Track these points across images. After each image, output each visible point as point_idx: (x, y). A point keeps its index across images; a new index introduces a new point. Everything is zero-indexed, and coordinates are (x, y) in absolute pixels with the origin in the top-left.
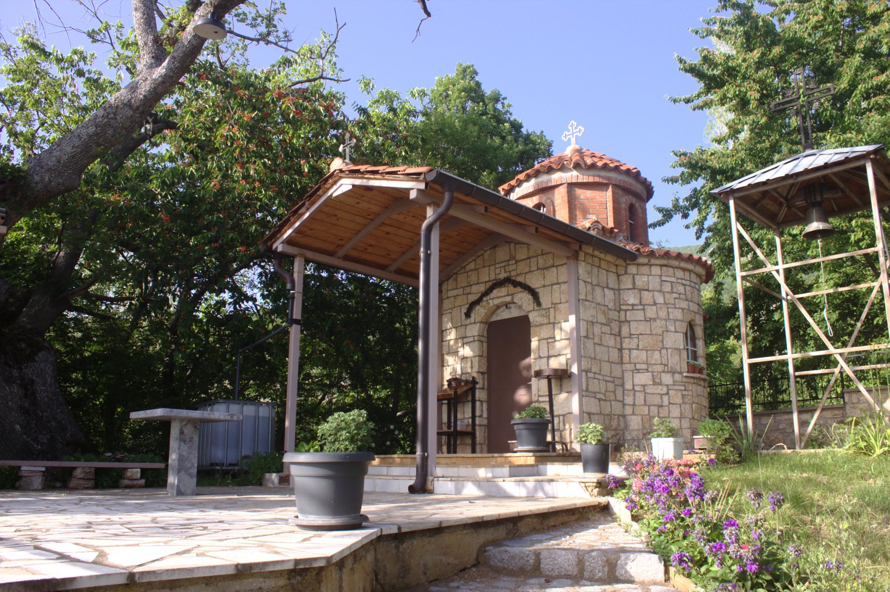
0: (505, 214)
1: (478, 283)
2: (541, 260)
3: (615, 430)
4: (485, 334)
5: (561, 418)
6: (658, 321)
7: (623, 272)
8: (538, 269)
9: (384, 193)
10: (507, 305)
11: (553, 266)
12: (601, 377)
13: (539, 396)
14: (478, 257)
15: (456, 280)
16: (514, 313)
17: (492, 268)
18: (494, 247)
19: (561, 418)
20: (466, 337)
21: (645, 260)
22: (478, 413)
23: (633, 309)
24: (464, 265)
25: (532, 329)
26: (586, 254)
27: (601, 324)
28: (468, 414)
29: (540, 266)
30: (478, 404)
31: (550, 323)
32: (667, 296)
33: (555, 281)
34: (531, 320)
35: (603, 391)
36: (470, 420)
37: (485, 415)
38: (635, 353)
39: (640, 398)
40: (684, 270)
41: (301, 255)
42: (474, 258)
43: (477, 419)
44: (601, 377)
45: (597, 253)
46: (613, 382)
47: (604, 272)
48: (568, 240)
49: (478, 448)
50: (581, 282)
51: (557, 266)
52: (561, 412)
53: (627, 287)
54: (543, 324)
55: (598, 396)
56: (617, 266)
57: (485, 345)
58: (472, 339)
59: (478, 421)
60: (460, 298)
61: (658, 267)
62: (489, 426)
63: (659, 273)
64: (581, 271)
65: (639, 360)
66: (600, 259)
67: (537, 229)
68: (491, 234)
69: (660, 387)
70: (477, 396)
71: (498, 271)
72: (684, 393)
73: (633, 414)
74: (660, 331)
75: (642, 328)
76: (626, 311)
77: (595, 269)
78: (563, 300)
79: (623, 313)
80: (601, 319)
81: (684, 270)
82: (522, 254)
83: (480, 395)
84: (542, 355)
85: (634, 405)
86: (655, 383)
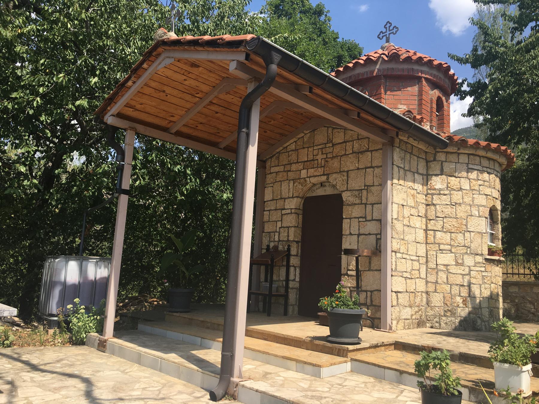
0: (329, 97)
1: (298, 162)
2: (356, 146)
3: (418, 306)
4: (301, 207)
5: (369, 293)
6: (463, 206)
7: (432, 159)
8: (353, 152)
9: (528, 320)
10: (322, 184)
12: (408, 257)
13: (348, 270)
14: (299, 139)
15: (278, 158)
16: (328, 191)
17: (310, 149)
18: (314, 130)
19: (369, 293)
20: (284, 209)
21: (454, 149)
22: (291, 277)
23: (440, 194)
24: (285, 145)
25: (344, 207)
26: (401, 140)
27: (411, 207)
28: (283, 276)
29: (355, 149)
30: (292, 269)
31: (362, 204)
32: (474, 182)
33: (369, 165)
34: (344, 200)
35: (409, 270)
36: (284, 283)
37: (297, 279)
38: (439, 234)
39: (443, 276)
40: (489, 159)
41: (132, 128)
42: (295, 139)
43: (291, 283)
44: (408, 257)
45: (411, 141)
46: (418, 261)
47: (415, 158)
48: (387, 126)
49: (290, 309)
50: (395, 167)
51: (372, 151)
52: (369, 288)
53: (435, 173)
54: (355, 204)
55: (405, 275)
56: (426, 152)
57: (301, 216)
58: (289, 211)
59: (291, 284)
61: (466, 155)
62: (301, 290)
63: (467, 161)
64: (396, 157)
65: (443, 241)
66: (412, 146)
67: (359, 113)
68: (311, 117)
69: (463, 268)
70: (291, 262)
71: (315, 152)
72: (484, 274)
73: (435, 291)
74: (463, 215)
75: (448, 210)
76: (433, 194)
77: (408, 156)
78: (376, 183)
79: (369, 207)
80: (411, 202)
81: (489, 159)
82: (339, 138)
83: (295, 261)
84: (352, 232)
85: (437, 282)
86: (457, 264)
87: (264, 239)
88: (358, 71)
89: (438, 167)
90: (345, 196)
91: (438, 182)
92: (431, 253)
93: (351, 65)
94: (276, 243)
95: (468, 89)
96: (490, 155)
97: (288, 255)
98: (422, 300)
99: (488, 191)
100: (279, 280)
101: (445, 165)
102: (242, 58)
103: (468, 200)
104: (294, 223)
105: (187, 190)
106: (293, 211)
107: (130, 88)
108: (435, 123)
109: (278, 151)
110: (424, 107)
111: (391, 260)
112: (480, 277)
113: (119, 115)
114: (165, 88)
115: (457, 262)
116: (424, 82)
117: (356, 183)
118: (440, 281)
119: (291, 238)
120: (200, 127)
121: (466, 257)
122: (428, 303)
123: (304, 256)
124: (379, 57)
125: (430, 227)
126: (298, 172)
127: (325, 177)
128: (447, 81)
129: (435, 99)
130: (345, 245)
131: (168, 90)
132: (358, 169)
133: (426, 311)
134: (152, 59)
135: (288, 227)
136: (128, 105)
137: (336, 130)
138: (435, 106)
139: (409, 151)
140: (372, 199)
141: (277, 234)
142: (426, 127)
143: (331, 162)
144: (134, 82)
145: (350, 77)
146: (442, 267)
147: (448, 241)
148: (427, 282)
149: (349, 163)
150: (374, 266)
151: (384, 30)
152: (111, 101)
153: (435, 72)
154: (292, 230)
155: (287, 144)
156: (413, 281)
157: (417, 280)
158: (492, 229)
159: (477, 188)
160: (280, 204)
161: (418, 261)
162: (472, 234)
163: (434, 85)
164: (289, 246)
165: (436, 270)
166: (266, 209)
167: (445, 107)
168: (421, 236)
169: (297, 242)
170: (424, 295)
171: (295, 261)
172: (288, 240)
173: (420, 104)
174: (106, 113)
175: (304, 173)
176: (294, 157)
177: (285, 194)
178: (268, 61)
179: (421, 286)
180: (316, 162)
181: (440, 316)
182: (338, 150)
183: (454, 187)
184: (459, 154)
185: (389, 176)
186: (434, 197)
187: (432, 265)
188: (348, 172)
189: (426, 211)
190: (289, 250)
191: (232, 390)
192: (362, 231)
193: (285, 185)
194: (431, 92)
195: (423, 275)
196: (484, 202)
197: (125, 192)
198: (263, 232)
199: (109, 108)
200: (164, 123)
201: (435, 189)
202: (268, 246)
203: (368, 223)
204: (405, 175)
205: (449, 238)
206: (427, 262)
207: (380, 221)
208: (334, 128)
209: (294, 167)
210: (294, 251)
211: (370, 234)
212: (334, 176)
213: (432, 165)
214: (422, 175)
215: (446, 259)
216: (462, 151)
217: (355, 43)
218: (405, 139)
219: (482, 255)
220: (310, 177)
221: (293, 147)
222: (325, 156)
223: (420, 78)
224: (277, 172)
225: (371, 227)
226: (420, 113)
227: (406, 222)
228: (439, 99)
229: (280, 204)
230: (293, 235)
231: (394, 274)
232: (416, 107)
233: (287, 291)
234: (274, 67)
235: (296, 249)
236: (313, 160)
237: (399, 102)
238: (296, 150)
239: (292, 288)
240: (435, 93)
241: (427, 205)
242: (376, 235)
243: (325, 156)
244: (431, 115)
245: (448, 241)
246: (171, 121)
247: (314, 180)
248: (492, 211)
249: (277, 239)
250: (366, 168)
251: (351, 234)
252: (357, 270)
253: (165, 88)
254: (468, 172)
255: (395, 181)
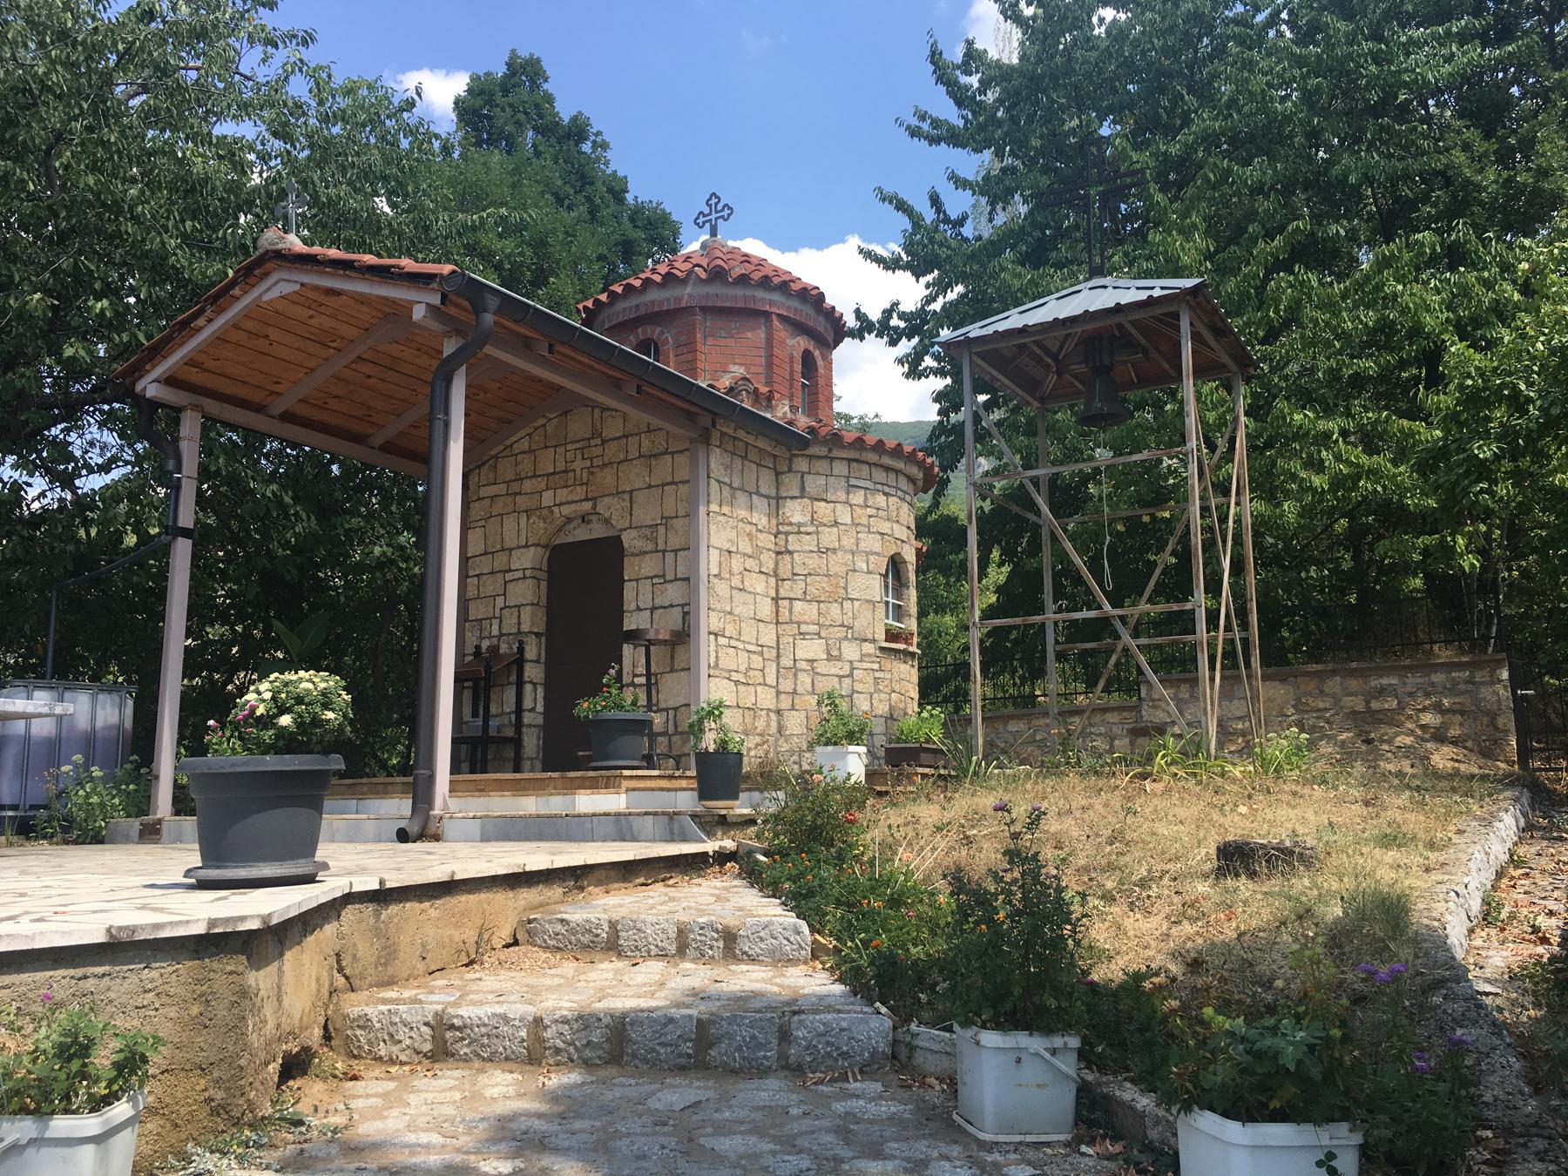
1: (535, 476)
4: (545, 567)
8: (641, 456)
10: (584, 519)
11: (666, 453)
12: (741, 646)
13: (635, 676)
16: (597, 531)
18: (566, 413)
20: (510, 571)
21: (823, 451)
22: (527, 704)
23: (799, 533)
24: (508, 442)
26: (723, 434)
28: (510, 704)
29: (644, 450)
30: (528, 688)
33: (669, 479)
34: (626, 545)
35: (743, 668)
37: (540, 708)
38: (798, 606)
39: (805, 680)
42: (528, 430)
43: (526, 714)
45: (741, 434)
46: (762, 653)
48: (694, 409)
51: (673, 453)
52: (671, 704)
53: (791, 494)
55: (735, 676)
57: (544, 585)
58: (520, 574)
59: (527, 718)
60: (500, 502)
64: (713, 465)
69: (839, 664)
71: (570, 456)
72: (877, 675)
73: (793, 708)
74: (841, 570)
75: (814, 562)
76: (787, 534)
77: (738, 462)
79: (670, 557)
81: (887, 469)
83: (533, 672)
85: (795, 692)
86: (830, 657)
87: (468, 634)
88: (653, 295)
89: (796, 482)
90: (628, 539)
91: (796, 512)
92: (783, 640)
93: (637, 283)
94: (495, 641)
95: (902, 324)
96: (886, 461)
97: (519, 661)
98: (768, 725)
99: (885, 527)
100: (503, 713)
101: (809, 479)
102: (436, 300)
103: (848, 542)
104: (530, 598)
105: (296, 535)
106: (528, 573)
107: (199, 330)
108: (798, 401)
109: (493, 453)
110: (776, 369)
111: (707, 649)
112: (870, 680)
113: (170, 381)
114: (270, 331)
115: (829, 654)
116: (776, 322)
117: (646, 513)
118: (800, 689)
119: (525, 628)
120: (332, 404)
121: (845, 644)
122: (780, 730)
123: (552, 663)
124: (690, 272)
125: (783, 593)
126: (537, 496)
127: (590, 504)
128: (822, 320)
129: (798, 355)
130: (629, 624)
131: (275, 335)
132: (650, 486)
133: (776, 745)
134: (251, 280)
135: (519, 607)
136: (191, 362)
137: (607, 414)
138: (798, 367)
139: (743, 454)
140: (674, 542)
141: (495, 622)
142: (781, 412)
143: (600, 475)
144: (210, 321)
145: (637, 306)
146: (803, 665)
147: (815, 617)
148: (778, 693)
149: (634, 476)
150: (678, 664)
151: (707, 211)
152: (156, 352)
153: (796, 304)
154: (526, 612)
155: (513, 439)
156: (752, 689)
157: (759, 688)
158: (898, 596)
159: (864, 521)
160: (500, 561)
161: (762, 653)
162: (856, 604)
163: (799, 328)
164: (521, 642)
165: (795, 671)
166: (471, 573)
167: (821, 371)
168: (766, 609)
169: (538, 635)
170: (773, 716)
171: (533, 672)
172: (519, 632)
173: (770, 365)
174: (141, 377)
175: (548, 498)
176: (526, 466)
177: (510, 539)
178: (478, 309)
179: (767, 699)
180: (571, 475)
181: (801, 751)
182: (612, 451)
183: (825, 520)
184: (832, 459)
185: (702, 498)
186: (790, 538)
187: (786, 661)
188: (631, 492)
189: (777, 564)
190: (521, 650)
191: (432, 829)
192: (658, 602)
193: (509, 522)
194: (791, 342)
195: (771, 680)
196: (877, 547)
197: (186, 533)
198: (467, 620)
199: (148, 367)
200: (256, 397)
201: (791, 524)
202: (478, 647)
203: (669, 586)
204: (733, 496)
205: (815, 611)
206: (778, 656)
207: (688, 579)
208: (604, 410)
209: (528, 485)
210: (531, 653)
211: (672, 606)
212: (607, 500)
213: (786, 479)
214: (768, 497)
215: (811, 649)
216: (835, 453)
217: (663, 210)
218: (730, 431)
219: (874, 641)
220: (561, 504)
221: (524, 444)
222: (588, 463)
223: (767, 315)
224: (492, 498)
225: (673, 593)
226: (769, 382)
227: (736, 582)
228: (807, 357)
229: (500, 561)
230: (532, 620)
231: (712, 672)
232: (761, 370)
233: (519, 732)
234: (489, 318)
235: (535, 649)
236: (565, 471)
237: (724, 366)
238: (531, 451)
239: (530, 726)
240: (801, 343)
241: (778, 553)
242: (683, 606)
243: (588, 463)
244: (792, 386)
245: (815, 617)
246: (272, 393)
247: (566, 510)
248: (896, 563)
249: (495, 632)
250: (664, 485)
251: (639, 609)
252: (648, 675)
253: (270, 331)
254: (848, 493)
255: (714, 507)
